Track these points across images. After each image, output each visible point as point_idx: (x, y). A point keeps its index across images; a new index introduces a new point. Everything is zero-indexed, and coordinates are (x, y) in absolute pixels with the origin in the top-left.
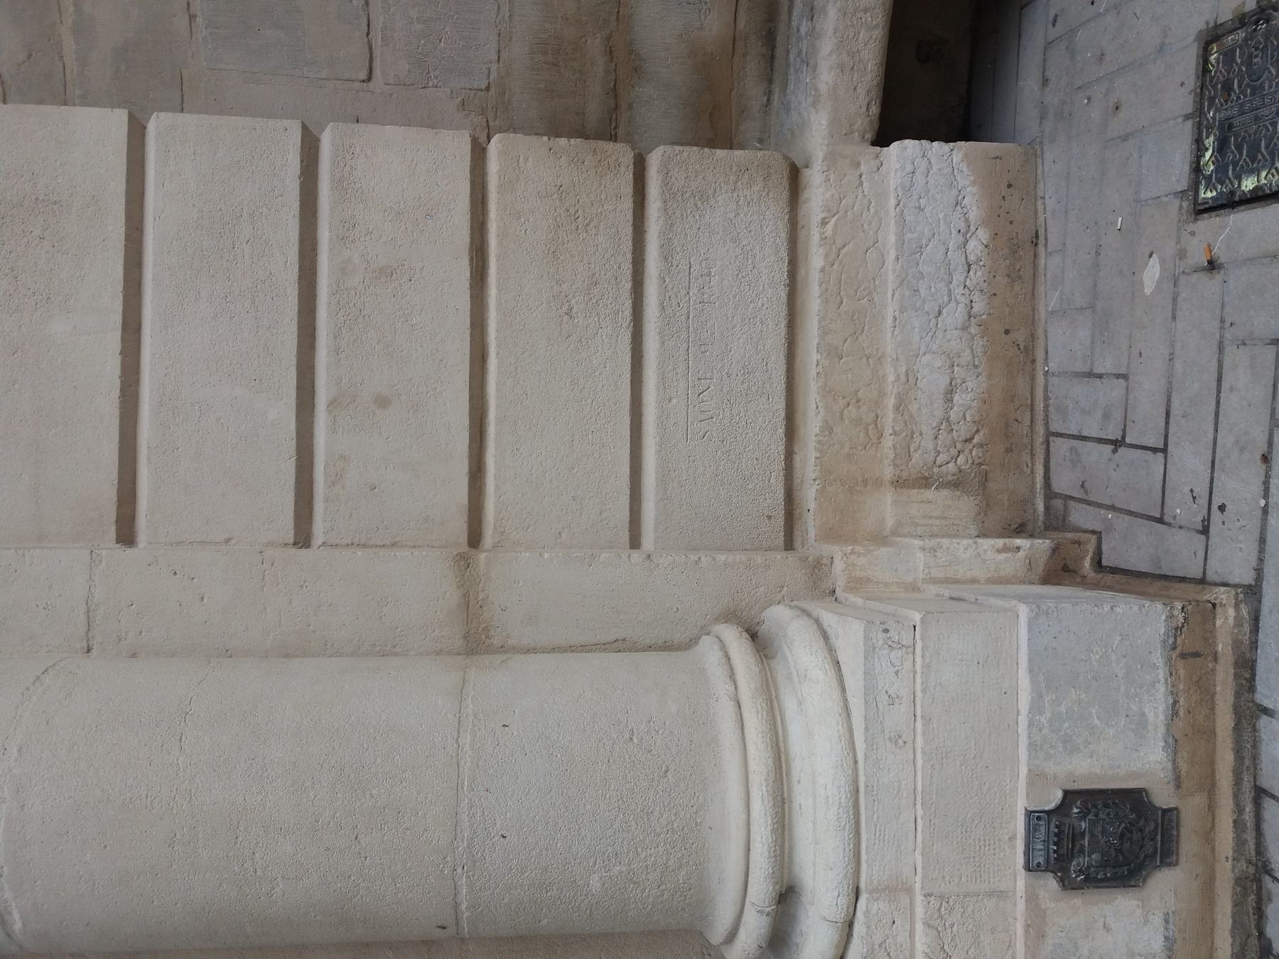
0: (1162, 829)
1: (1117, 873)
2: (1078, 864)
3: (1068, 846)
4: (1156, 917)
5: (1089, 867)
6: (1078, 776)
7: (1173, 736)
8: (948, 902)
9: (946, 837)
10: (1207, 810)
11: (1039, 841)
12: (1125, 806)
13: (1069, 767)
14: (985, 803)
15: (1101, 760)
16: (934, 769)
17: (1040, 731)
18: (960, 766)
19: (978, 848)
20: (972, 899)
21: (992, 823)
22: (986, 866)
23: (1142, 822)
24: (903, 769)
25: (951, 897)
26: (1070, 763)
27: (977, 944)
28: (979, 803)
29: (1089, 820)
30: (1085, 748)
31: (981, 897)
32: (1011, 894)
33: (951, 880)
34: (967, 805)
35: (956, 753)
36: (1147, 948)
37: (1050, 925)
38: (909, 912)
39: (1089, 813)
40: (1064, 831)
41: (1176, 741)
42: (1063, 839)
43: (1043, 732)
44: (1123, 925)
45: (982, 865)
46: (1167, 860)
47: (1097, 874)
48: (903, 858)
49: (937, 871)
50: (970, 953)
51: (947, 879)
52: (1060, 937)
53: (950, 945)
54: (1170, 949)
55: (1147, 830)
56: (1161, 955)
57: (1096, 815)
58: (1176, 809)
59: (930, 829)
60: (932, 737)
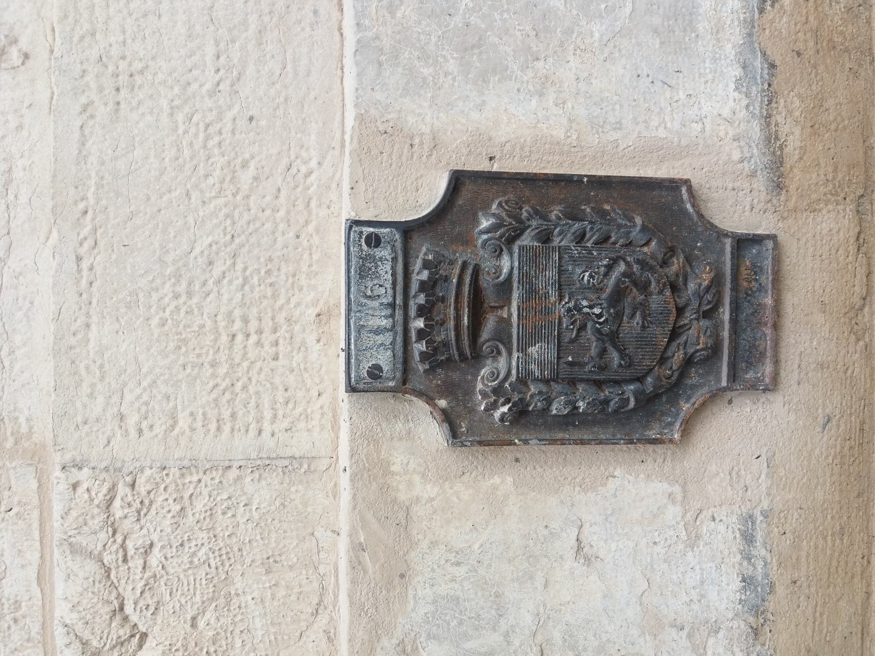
0: (735, 288)
1: (606, 402)
2: (494, 375)
3: (458, 318)
4: (722, 528)
5: (522, 382)
6: (503, 145)
7: (764, 54)
8: (133, 485)
9: (129, 307)
10: (852, 249)
11: (375, 304)
12: (631, 219)
13: (475, 115)
14: (246, 217)
15: (569, 105)
16: (92, 117)
17: (393, 14)
18: (172, 115)
19: (224, 339)
20: (206, 478)
21: (268, 272)
22: (252, 389)
23: (676, 264)
24: (20, 128)
25: (142, 470)
26: (480, 107)
27: (222, 601)
28: (227, 216)
29: (521, 248)
30: (524, 68)
31: (233, 474)
32: (323, 464)
33: (144, 425)
34: (191, 220)
35: (160, 77)
36: (695, 607)
37: (425, 545)
38: (36, 514)
39: (522, 232)
40: (446, 279)
41: (772, 66)
42: (443, 299)
43: (399, 14)
44: (631, 545)
45: (239, 385)
46: (750, 375)
47: (549, 401)
48: (17, 368)
49: (100, 400)
50: (201, 624)
51: (132, 420)
52: (453, 580)
53: (141, 604)
54: (757, 610)
55: (692, 286)
56: (735, 624)
57: (545, 238)
58: (773, 238)
59: (78, 281)
60: (87, 26)
